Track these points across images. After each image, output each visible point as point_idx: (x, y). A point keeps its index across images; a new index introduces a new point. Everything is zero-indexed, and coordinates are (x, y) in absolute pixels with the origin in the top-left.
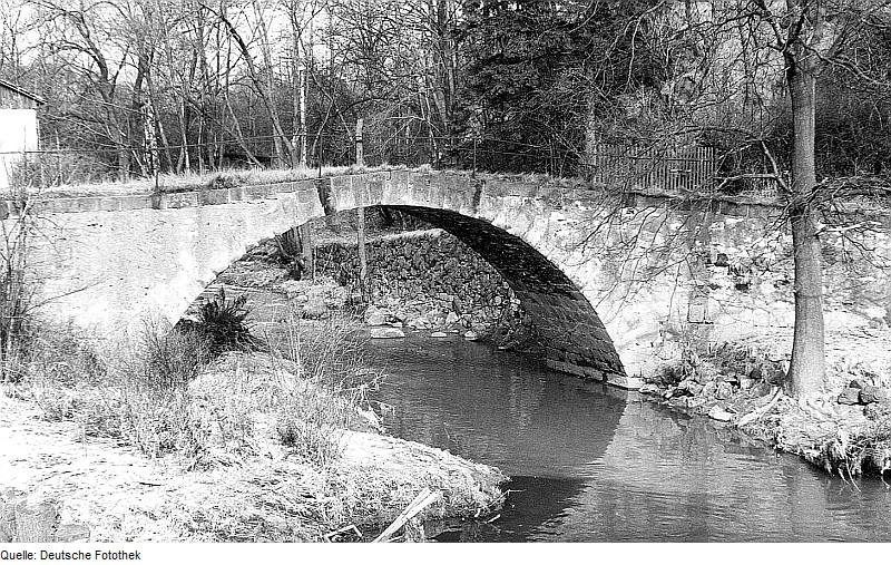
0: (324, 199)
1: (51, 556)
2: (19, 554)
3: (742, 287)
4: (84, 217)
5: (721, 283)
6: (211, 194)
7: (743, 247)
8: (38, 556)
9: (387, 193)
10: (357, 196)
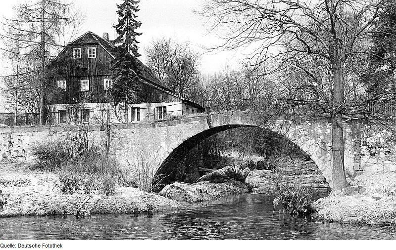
0: (209, 124)
1: (23, 246)
2: (8, 245)
3: (372, 155)
4: (129, 130)
5: (365, 153)
6: (171, 122)
7: (372, 138)
8: (17, 246)
9: (231, 120)
10: (221, 122)
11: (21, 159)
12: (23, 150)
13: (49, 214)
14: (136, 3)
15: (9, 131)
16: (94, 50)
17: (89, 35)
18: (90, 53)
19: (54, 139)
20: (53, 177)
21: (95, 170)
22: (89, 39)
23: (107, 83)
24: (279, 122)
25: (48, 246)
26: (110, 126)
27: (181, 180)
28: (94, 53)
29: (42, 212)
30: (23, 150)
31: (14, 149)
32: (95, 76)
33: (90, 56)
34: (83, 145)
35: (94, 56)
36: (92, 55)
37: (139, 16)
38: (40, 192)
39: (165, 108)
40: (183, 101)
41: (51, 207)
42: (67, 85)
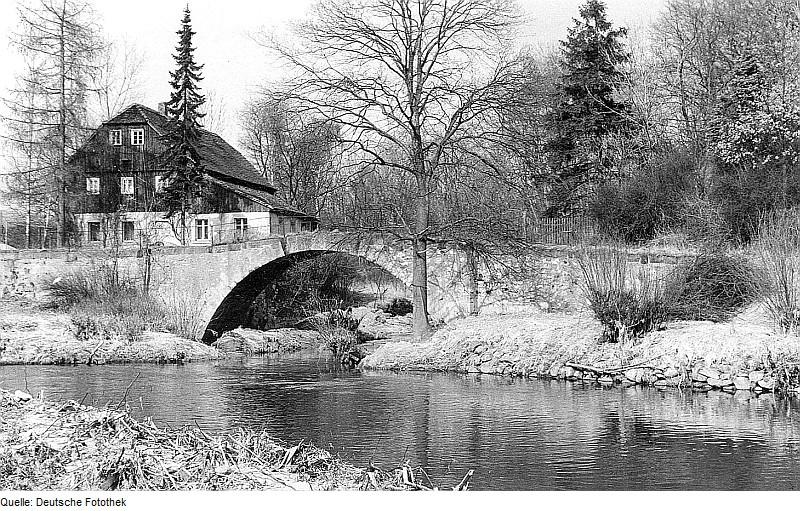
1: (46, 503)
2: (17, 502)
8: (34, 503)
11: (29, 296)
12: (32, 284)
13: (57, 363)
14: (198, 69)
15: (12, 257)
16: (140, 133)
17: (134, 110)
18: (135, 138)
19: (73, 268)
20: (64, 318)
21: (121, 310)
22: (134, 115)
23: (159, 183)
24: (379, 245)
25: (97, 502)
26: (150, 250)
27: (248, 325)
28: (140, 138)
29: (48, 360)
30: (32, 284)
31: (19, 281)
32: (143, 172)
33: (135, 142)
34: (112, 277)
35: (140, 142)
36: (138, 139)
37: (203, 88)
38: (48, 338)
39: (245, 221)
40: (271, 211)
41: (59, 355)
42: (101, 185)
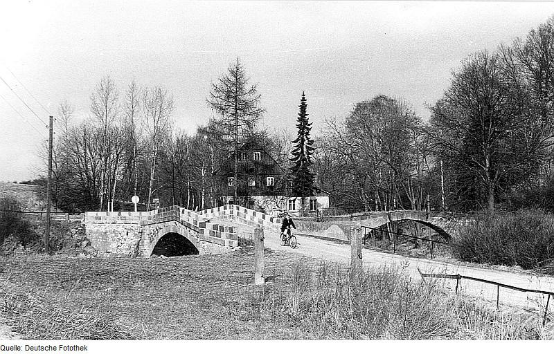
2: (12, 347)
8: (23, 348)
14: (309, 125)
25: (68, 348)
39: (315, 201)
